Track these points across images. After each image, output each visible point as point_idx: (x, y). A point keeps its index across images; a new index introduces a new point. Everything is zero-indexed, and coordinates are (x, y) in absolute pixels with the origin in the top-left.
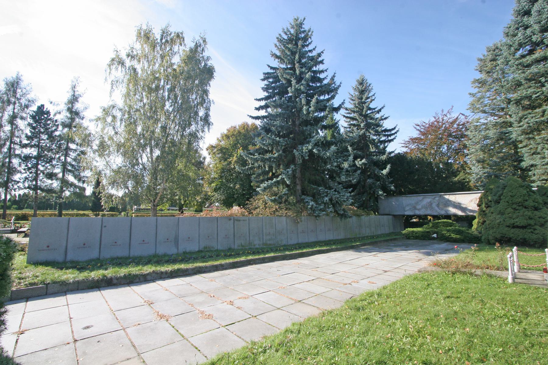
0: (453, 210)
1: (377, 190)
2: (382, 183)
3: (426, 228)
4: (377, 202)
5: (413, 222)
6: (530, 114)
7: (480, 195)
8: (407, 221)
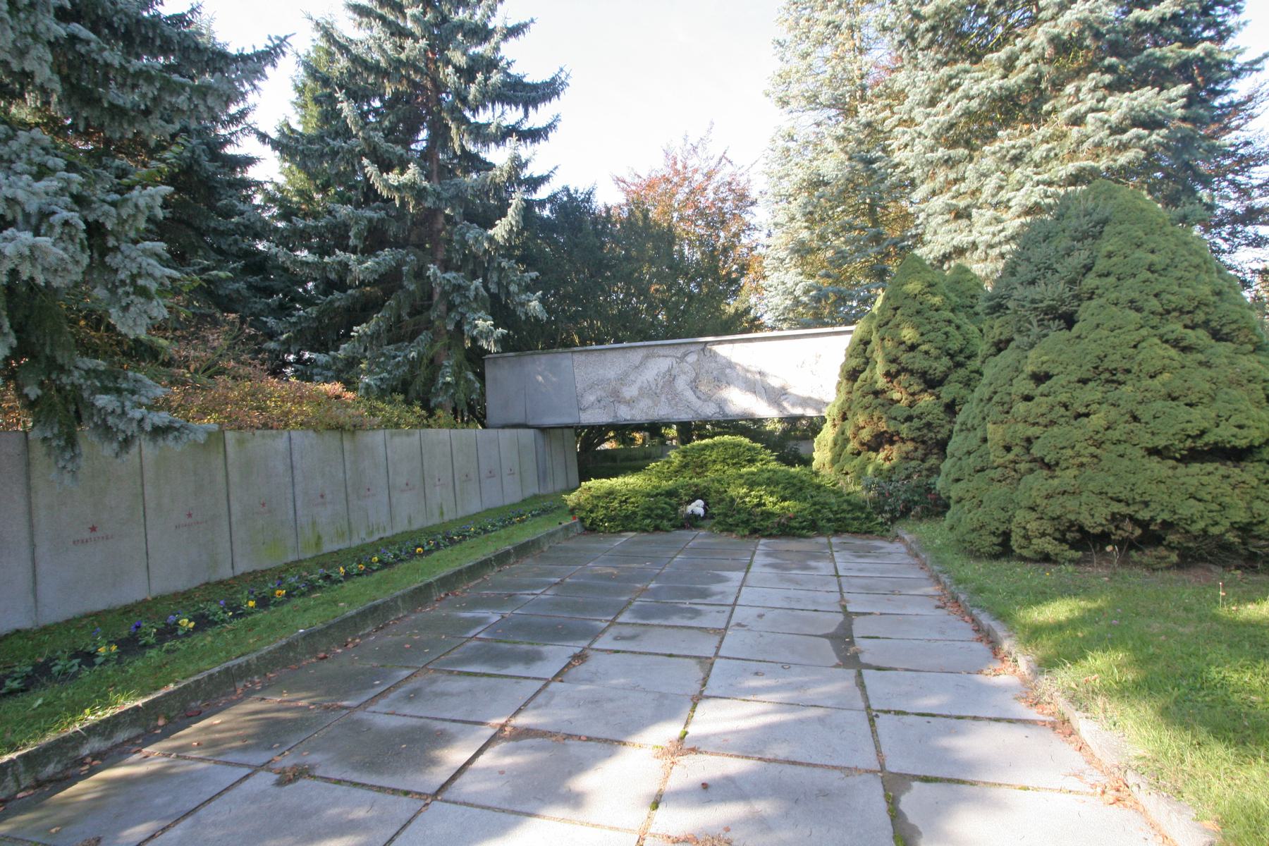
0: (740, 402)
1: (470, 315)
2: (493, 288)
3: (660, 475)
4: (481, 377)
5: (607, 450)
6: (966, 71)
7: (848, 338)
8: (594, 450)
